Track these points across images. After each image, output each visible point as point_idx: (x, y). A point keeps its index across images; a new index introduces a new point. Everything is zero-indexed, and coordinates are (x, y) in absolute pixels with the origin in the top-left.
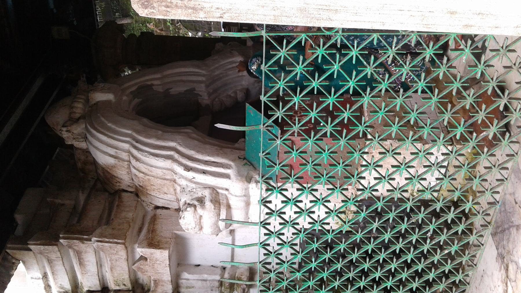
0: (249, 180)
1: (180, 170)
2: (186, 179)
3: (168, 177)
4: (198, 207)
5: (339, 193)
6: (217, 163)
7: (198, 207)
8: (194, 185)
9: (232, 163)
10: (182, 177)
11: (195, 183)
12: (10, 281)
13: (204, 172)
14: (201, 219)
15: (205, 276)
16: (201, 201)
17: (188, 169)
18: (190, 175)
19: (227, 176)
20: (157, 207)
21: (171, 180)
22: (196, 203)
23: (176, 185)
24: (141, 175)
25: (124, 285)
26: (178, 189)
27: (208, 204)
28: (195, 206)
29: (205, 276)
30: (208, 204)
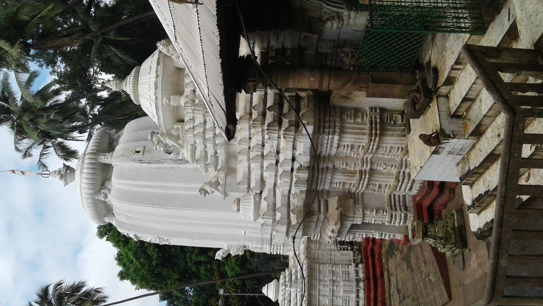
0: (351, 10)
1: (324, 5)
2: (327, 9)
3: (319, 7)
4: (333, 20)
5: (461, 147)
6: (338, 2)
7: (333, 20)
8: (329, 11)
9: (344, 3)
10: (325, 8)
11: (331, 10)
12: (240, 45)
13: (334, 6)
14: (469, 107)
15: (328, 44)
16: (333, 17)
17: (328, 5)
18: (329, 7)
19: (342, 8)
20: (310, 17)
21: (320, 8)
22: (332, 19)
23: (322, 10)
24: (308, 6)
25: (295, 47)
26: (323, 12)
27: (336, 19)
28: (331, 20)
29: (328, 44)
30: (336, 19)
